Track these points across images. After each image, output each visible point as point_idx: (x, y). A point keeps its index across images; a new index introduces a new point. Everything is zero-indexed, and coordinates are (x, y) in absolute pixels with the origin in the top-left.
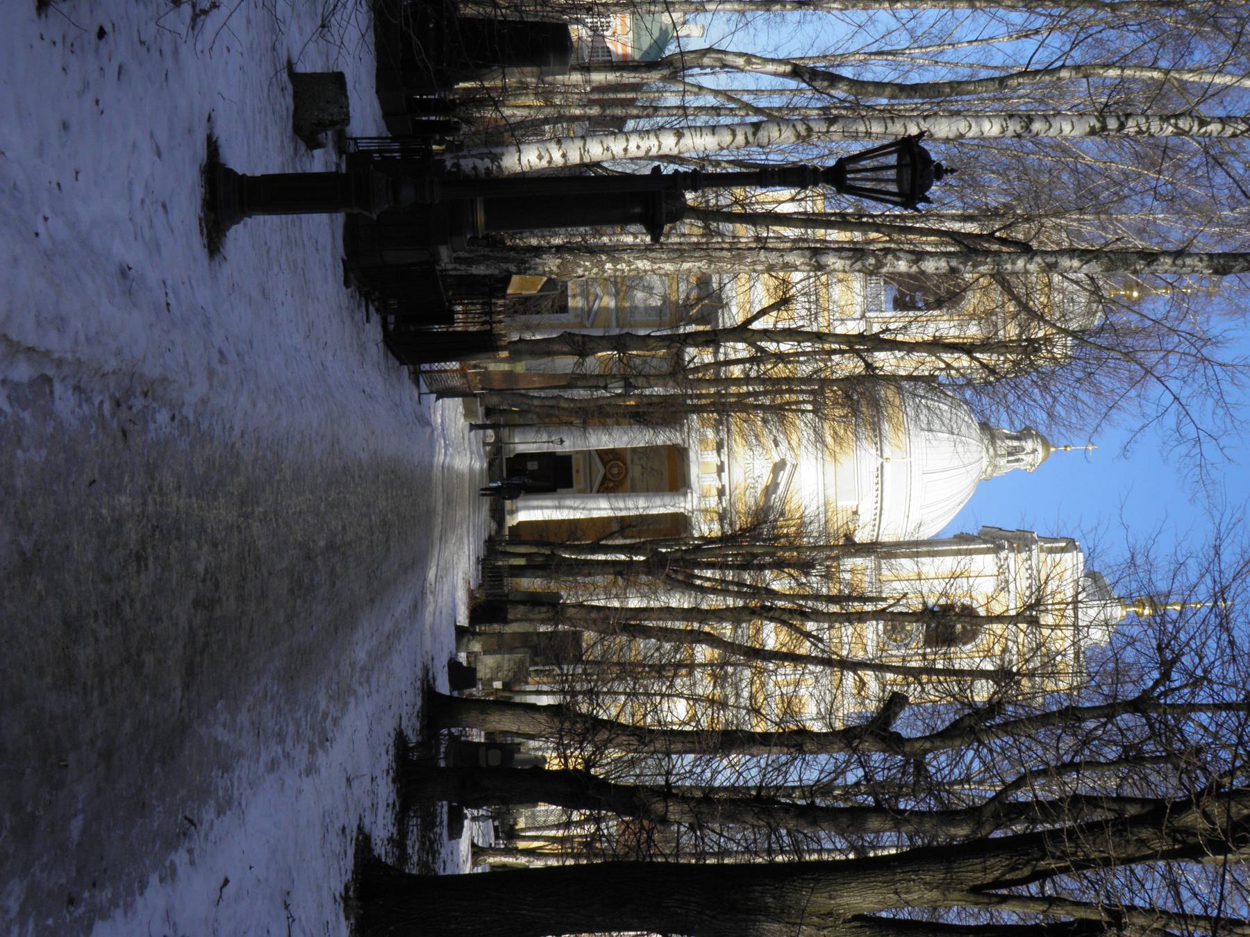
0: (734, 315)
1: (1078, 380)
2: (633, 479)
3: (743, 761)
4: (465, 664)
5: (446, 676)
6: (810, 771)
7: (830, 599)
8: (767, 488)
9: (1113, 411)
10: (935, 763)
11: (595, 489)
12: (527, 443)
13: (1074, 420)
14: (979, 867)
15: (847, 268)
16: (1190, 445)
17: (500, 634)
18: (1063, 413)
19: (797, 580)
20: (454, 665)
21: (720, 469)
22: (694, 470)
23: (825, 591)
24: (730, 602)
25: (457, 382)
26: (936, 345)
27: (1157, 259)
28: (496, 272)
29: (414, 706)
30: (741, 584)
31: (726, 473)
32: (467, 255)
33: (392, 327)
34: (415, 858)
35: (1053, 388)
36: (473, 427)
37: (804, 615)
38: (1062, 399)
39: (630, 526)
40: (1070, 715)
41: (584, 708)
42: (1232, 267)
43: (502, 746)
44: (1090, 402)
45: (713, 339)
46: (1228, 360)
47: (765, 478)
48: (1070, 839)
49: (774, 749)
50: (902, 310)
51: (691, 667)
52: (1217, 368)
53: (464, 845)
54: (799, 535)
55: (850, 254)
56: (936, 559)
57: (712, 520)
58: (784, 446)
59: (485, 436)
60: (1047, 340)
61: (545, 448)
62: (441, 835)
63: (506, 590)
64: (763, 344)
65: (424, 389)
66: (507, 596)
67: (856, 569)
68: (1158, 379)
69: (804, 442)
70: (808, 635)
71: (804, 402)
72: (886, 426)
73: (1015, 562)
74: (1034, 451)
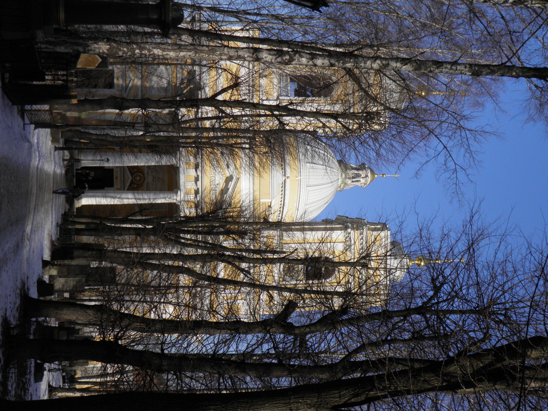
0: (208, 92)
1: (393, 136)
2: (148, 184)
3: (205, 337)
4: (47, 282)
5: (36, 289)
6: (240, 346)
7: (255, 252)
8: (222, 190)
9: (412, 152)
10: (311, 340)
11: (126, 188)
12: (88, 161)
13: (390, 158)
14: (337, 395)
15: (273, 61)
16: (451, 172)
17: (69, 266)
18: (384, 153)
19: (237, 241)
20: (40, 282)
21: (197, 179)
22: (182, 179)
23: (252, 247)
24: (200, 251)
25: (47, 117)
26: (317, 114)
27: (442, 65)
28: (71, 51)
29: (15, 304)
30: (206, 242)
31: (199, 181)
32: (53, 40)
33: (7, 80)
34: (13, 393)
35: (380, 140)
36: (56, 149)
37: (242, 259)
38: (384, 145)
39: (145, 209)
40: (385, 315)
41: (115, 307)
42: (482, 72)
43: (68, 328)
44: (400, 149)
45: (194, 102)
46: (473, 128)
47: (221, 186)
48: (389, 380)
49: (223, 331)
50: (299, 96)
51: (177, 287)
52: (467, 132)
53: (44, 386)
54: (239, 216)
55: (275, 53)
56: (314, 233)
57: (191, 207)
58: (232, 168)
59: (64, 155)
60: (378, 113)
61: (97, 164)
62: (30, 379)
63: (73, 242)
64: (224, 108)
65: (27, 121)
66: (73, 244)
67: (270, 237)
68: (436, 136)
69: (244, 165)
70: (242, 270)
71: (245, 143)
72: (288, 158)
73: (354, 234)
74: (367, 176)
